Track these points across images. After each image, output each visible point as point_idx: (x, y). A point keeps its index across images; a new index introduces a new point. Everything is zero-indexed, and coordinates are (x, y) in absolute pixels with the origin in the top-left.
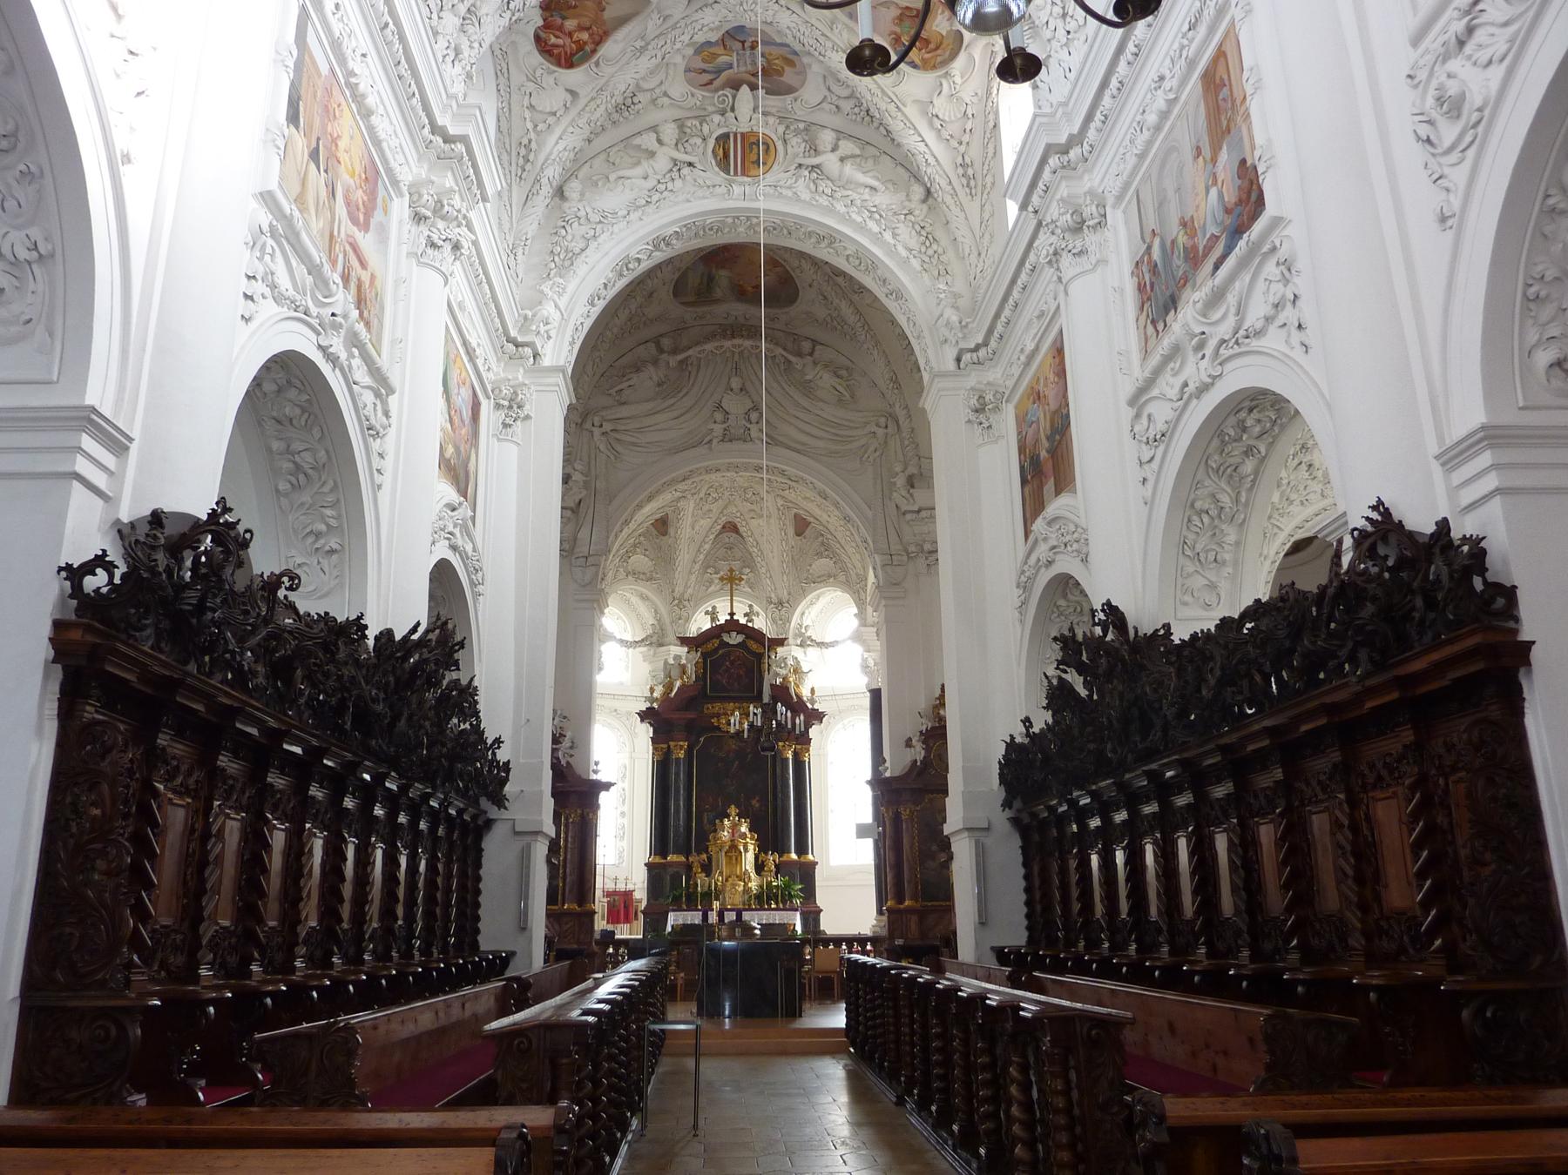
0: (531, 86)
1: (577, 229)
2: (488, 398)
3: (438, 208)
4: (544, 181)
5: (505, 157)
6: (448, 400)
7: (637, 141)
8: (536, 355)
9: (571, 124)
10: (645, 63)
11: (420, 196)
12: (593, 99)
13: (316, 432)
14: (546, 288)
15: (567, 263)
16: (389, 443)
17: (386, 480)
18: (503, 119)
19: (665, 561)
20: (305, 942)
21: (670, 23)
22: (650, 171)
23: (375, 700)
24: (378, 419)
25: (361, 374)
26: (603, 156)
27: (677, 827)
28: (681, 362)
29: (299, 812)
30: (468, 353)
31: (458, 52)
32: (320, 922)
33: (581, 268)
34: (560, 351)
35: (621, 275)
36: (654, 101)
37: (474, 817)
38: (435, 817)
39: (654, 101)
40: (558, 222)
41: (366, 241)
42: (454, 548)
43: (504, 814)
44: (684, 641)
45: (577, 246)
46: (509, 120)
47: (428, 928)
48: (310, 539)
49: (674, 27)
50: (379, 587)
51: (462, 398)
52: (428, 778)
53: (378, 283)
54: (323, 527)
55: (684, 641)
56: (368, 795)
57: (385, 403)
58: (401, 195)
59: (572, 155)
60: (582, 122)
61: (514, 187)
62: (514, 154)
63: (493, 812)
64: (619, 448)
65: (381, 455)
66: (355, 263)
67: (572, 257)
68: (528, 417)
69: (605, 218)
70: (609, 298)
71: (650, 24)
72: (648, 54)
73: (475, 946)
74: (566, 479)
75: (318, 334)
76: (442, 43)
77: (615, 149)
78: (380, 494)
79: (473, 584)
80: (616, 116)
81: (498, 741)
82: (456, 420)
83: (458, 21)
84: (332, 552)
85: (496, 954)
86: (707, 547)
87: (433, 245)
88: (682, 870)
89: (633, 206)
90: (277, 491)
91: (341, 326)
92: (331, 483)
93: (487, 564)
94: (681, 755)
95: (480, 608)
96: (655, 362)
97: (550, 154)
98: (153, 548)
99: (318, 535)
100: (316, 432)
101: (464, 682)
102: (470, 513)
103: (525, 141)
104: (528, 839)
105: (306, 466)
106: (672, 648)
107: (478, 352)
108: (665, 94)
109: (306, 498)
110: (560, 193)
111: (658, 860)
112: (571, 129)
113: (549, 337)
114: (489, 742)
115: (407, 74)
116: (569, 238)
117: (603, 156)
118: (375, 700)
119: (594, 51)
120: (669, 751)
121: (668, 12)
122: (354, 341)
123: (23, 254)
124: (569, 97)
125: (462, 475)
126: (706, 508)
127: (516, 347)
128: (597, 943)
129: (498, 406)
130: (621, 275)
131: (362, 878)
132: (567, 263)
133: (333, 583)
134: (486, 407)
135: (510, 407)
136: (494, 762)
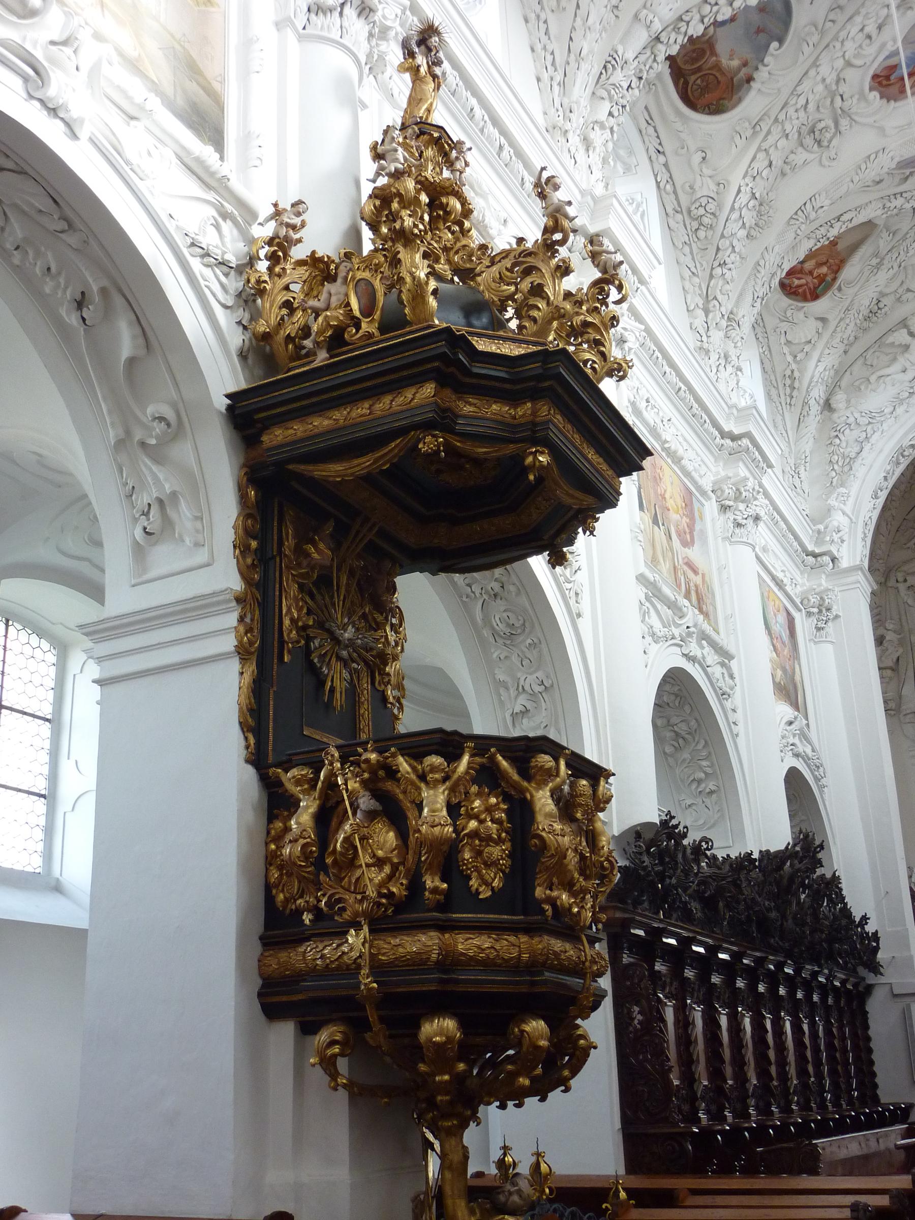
0: (784, 326)
1: (850, 435)
2: (800, 610)
3: (738, 497)
4: (812, 402)
5: (774, 392)
6: (770, 633)
7: (890, 339)
8: (834, 559)
9: (826, 347)
10: (883, 276)
11: (723, 491)
12: (841, 320)
13: (687, 709)
14: (832, 502)
15: (846, 469)
16: (737, 699)
17: (740, 729)
18: (766, 361)
20: (703, 1098)
21: (898, 237)
22: (908, 365)
23: (769, 910)
24: (724, 684)
25: (712, 658)
26: (861, 361)
29: (733, 1000)
30: (777, 584)
31: (726, 357)
32: (758, 1080)
33: (859, 469)
34: (854, 550)
35: (898, 463)
36: (899, 300)
37: (856, 985)
38: (824, 990)
39: (899, 300)
40: (831, 434)
41: (694, 554)
42: (797, 755)
45: (852, 451)
46: (771, 360)
47: (835, 1085)
48: (694, 786)
49: (904, 238)
50: (751, 814)
51: (779, 624)
52: (816, 960)
53: (707, 579)
54: (702, 775)
56: (773, 980)
57: (729, 669)
58: (710, 499)
59: (832, 372)
60: (836, 341)
61: (787, 415)
62: (781, 386)
63: (871, 979)
65: (734, 710)
66: (690, 574)
67: (850, 462)
69: (872, 418)
70: (890, 487)
71: (882, 243)
72: (884, 268)
73: (876, 1100)
74: (879, 641)
75: (681, 646)
76: (714, 356)
77: (871, 351)
78: (738, 740)
79: (818, 780)
80: (865, 324)
81: (865, 919)
82: (778, 645)
83: (721, 334)
84: (711, 792)
85: (897, 1106)
87: (739, 525)
89: (899, 401)
90: (665, 753)
91: (694, 633)
92: (702, 743)
93: (826, 761)
95: (826, 797)
97: (812, 377)
98: (641, 854)
99: (699, 782)
100: (687, 709)
101: (829, 875)
102: (805, 722)
103: (788, 373)
104: (907, 1000)
105: (683, 733)
107: (785, 580)
108: (909, 290)
109: (686, 755)
110: (828, 406)
112: (827, 351)
113: (842, 541)
114: (857, 920)
116: (844, 444)
117: (861, 361)
118: (769, 910)
119: (834, 279)
121: (894, 229)
122: (704, 636)
123: (538, 689)
124: (820, 324)
125: (791, 688)
127: (815, 559)
129: (809, 614)
130: (898, 463)
131: (781, 1047)
132: (846, 469)
133: (716, 816)
134: (798, 617)
135: (820, 611)
136: (864, 936)
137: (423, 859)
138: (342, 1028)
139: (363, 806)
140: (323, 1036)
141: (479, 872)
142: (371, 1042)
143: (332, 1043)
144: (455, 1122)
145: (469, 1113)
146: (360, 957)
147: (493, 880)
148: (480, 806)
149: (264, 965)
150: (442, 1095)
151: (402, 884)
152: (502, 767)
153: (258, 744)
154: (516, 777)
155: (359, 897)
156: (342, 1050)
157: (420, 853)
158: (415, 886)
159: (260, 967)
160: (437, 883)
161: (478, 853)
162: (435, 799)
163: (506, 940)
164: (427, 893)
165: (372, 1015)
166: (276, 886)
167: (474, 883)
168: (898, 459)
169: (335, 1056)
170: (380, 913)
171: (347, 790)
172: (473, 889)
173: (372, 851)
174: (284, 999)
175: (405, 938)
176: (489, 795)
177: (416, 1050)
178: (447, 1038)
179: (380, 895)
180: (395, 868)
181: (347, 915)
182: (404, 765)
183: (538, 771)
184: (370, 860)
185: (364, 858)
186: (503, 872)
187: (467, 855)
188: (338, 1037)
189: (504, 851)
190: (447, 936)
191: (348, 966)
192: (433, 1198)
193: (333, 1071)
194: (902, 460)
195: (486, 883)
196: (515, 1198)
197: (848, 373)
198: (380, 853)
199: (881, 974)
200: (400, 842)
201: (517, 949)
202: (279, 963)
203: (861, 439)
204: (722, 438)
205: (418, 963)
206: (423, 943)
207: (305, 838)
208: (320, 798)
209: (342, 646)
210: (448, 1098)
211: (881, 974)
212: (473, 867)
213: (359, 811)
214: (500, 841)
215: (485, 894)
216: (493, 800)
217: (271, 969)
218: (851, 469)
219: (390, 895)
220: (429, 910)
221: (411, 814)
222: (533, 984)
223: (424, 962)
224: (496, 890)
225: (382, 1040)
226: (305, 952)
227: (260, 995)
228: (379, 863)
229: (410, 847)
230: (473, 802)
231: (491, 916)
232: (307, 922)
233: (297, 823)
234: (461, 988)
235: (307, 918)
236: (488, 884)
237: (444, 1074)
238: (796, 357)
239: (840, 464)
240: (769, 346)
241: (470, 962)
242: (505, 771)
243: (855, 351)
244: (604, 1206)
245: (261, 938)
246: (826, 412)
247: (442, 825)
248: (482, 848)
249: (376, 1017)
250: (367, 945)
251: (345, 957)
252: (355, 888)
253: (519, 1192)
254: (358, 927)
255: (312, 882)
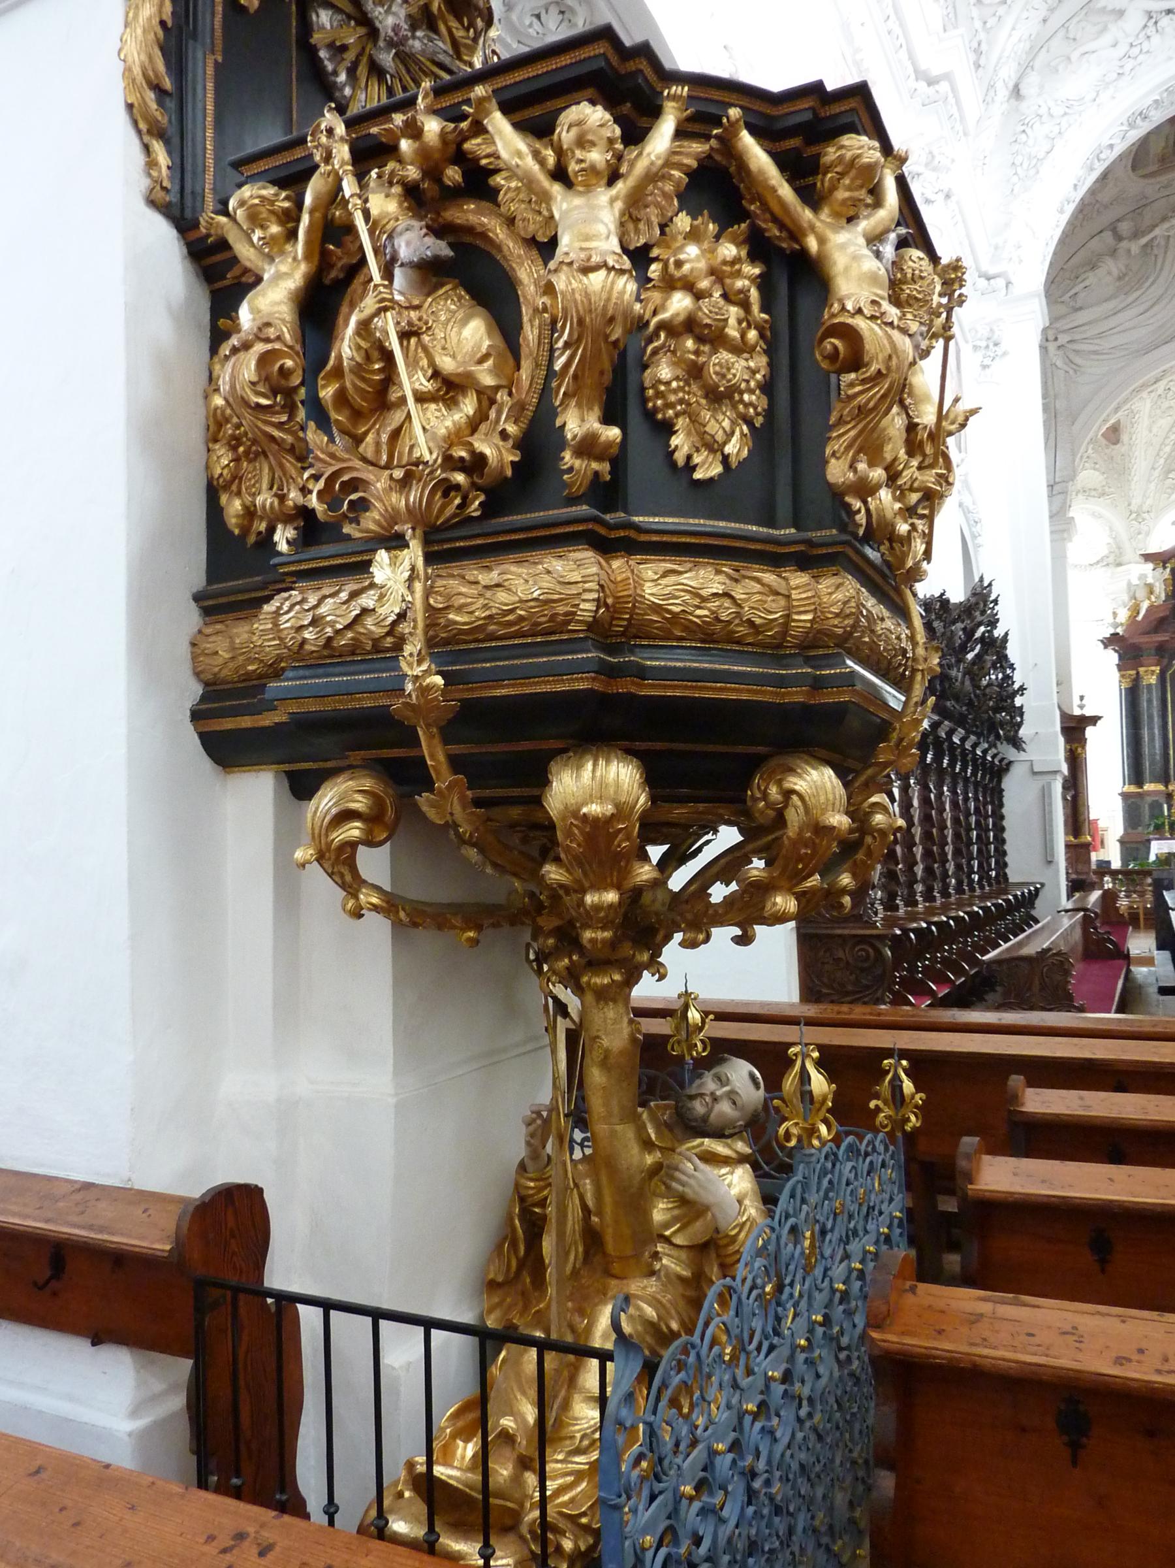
2: (967, 342)
4: (999, 85)
15: (1032, 172)
19: (1119, 472)
26: (1061, 33)
27: (1152, 755)
28: (1146, 245)
35: (1092, 169)
43: (1022, 756)
44: (1148, 557)
55: (1148, 557)
59: (1028, 45)
63: (1010, 753)
64: (1078, 360)
68: (1005, 354)
73: (1002, 877)
86: (1168, 449)
88: (1162, 799)
94: (1153, 680)
96: (1113, 253)
104: (1047, 778)
106: (1132, 566)
110: (1016, 92)
111: (1133, 789)
112: (1026, 14)
115: (897, 30)
117: (1061, 33)
120: (1137, 679)
126: (1166, 404)
128: (1095, 872)
129: (976, 348)
132: (1032, 172)
137: (558, 365)
138: (368, 784)
139: (404, 253)
140: (327, 800)
141: (694, 419)
142: (431, 814)
143: (345, 816)
144: (617, 977)
145: (645, 957)
146: (402, 616)
147: (729, 435)
148: (697, 259)
149: (204, 654)
150: (594, 928)
151: (504, 435)
152: (753, 166)
153: (180, 168)
154: (786, 191)
155: (398, 474)
156: (369, 832)
157: (552, 350)
158: (538, 442)
159: (194, 658)
160: (593, 423)
161: (695, 372)
162: (590, 224)
163: (758, 580)
164: (567, 455)
165: (434, 753)
166: (227, 487)
167: (680, 442)
168: (1092, 163)
169: (352, 845)
170: (451, 510)
171: (367, 214)
172: (680, 457)
173: (432, 363)
174: (246, 722)
175: (513, 568)
176: (717, 237)
177: (540, 835)
178: (617, 806)
179: (450, 462)
180: (487, 398)
181: (371, 521)
182: (506, 141)
183: (842, 175)
184: (427, 386)
185: (411, 380)
186: (749, 422)
187: (665, 371)
188: (360, 804)
189: (754, 372)
190: (616, 564)
191: (376, 642)
192: (566, 1116)
193: (348, 878)
194: (1097, 164)
195: (714, 442)
196: (725, 1107)
197: (1044, 50)
198: (447, 364)
199: (1024, 750)
200: (499, 342)
201: (783, 602)
202: (233, 648)
203: (1052, 135)
204: (917, 79)
205: (546, 631)
206: (564, 578)
207: (267, 340)
208: (307, 257)
209: (381, 44)
210: (607, 934)
211: (1024, 750)
212: (681, 401)
213: (398, 272)
214: (741, 349)
215: (708, 469)
216: (728, 250)
217: (220, 661)
218: (1038, 172)
219: (477, 463)
220: (572, 501)
221: (527, 273)
222: (818, 684)
223: (559, 624)
224: (734, 463)
225: (457, 809)
226: (277, 613)
227: (196, 716)
228: (449, 388)
229: (524, 351)
230: (681, 249)
231: (722, 524)
232: (283, 547)
233: (254, 310)
234: (650, 689)
235: (283, 537)
236: (713, 447)
237: (606, 889)
238: (985, 23)
239: (1025, 165)
240: (954, 7)
241: (676, 629)
242: (761, 172)
243: (1056, 20)
244: (872, 1104)
245: (198, 598)
246: (1013, 101)
247: (610, 269)
248: (702, 359)
249: (442, 758)
250: (418, 586)
251: (369, 622)
252: (391, 456)
253: (732, 1096)
254: (395, 542)
255: (292, 450)
